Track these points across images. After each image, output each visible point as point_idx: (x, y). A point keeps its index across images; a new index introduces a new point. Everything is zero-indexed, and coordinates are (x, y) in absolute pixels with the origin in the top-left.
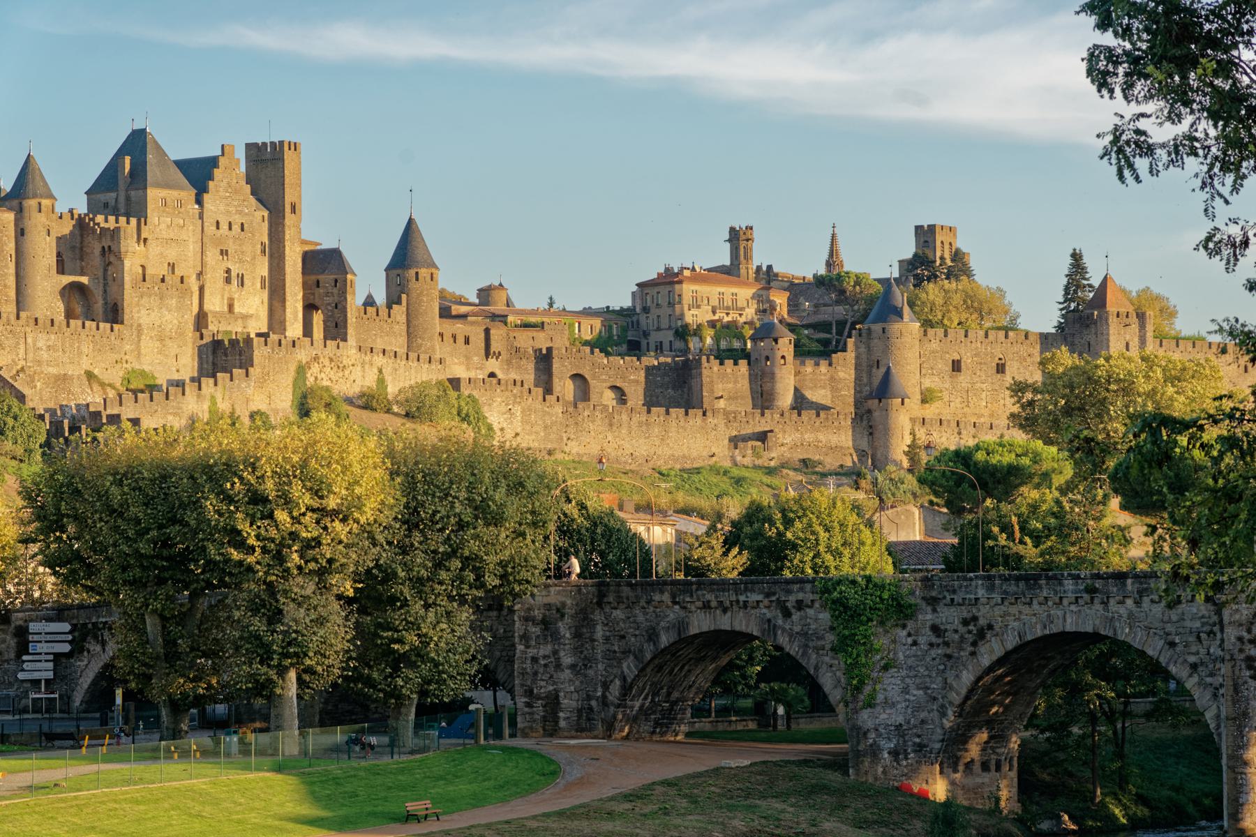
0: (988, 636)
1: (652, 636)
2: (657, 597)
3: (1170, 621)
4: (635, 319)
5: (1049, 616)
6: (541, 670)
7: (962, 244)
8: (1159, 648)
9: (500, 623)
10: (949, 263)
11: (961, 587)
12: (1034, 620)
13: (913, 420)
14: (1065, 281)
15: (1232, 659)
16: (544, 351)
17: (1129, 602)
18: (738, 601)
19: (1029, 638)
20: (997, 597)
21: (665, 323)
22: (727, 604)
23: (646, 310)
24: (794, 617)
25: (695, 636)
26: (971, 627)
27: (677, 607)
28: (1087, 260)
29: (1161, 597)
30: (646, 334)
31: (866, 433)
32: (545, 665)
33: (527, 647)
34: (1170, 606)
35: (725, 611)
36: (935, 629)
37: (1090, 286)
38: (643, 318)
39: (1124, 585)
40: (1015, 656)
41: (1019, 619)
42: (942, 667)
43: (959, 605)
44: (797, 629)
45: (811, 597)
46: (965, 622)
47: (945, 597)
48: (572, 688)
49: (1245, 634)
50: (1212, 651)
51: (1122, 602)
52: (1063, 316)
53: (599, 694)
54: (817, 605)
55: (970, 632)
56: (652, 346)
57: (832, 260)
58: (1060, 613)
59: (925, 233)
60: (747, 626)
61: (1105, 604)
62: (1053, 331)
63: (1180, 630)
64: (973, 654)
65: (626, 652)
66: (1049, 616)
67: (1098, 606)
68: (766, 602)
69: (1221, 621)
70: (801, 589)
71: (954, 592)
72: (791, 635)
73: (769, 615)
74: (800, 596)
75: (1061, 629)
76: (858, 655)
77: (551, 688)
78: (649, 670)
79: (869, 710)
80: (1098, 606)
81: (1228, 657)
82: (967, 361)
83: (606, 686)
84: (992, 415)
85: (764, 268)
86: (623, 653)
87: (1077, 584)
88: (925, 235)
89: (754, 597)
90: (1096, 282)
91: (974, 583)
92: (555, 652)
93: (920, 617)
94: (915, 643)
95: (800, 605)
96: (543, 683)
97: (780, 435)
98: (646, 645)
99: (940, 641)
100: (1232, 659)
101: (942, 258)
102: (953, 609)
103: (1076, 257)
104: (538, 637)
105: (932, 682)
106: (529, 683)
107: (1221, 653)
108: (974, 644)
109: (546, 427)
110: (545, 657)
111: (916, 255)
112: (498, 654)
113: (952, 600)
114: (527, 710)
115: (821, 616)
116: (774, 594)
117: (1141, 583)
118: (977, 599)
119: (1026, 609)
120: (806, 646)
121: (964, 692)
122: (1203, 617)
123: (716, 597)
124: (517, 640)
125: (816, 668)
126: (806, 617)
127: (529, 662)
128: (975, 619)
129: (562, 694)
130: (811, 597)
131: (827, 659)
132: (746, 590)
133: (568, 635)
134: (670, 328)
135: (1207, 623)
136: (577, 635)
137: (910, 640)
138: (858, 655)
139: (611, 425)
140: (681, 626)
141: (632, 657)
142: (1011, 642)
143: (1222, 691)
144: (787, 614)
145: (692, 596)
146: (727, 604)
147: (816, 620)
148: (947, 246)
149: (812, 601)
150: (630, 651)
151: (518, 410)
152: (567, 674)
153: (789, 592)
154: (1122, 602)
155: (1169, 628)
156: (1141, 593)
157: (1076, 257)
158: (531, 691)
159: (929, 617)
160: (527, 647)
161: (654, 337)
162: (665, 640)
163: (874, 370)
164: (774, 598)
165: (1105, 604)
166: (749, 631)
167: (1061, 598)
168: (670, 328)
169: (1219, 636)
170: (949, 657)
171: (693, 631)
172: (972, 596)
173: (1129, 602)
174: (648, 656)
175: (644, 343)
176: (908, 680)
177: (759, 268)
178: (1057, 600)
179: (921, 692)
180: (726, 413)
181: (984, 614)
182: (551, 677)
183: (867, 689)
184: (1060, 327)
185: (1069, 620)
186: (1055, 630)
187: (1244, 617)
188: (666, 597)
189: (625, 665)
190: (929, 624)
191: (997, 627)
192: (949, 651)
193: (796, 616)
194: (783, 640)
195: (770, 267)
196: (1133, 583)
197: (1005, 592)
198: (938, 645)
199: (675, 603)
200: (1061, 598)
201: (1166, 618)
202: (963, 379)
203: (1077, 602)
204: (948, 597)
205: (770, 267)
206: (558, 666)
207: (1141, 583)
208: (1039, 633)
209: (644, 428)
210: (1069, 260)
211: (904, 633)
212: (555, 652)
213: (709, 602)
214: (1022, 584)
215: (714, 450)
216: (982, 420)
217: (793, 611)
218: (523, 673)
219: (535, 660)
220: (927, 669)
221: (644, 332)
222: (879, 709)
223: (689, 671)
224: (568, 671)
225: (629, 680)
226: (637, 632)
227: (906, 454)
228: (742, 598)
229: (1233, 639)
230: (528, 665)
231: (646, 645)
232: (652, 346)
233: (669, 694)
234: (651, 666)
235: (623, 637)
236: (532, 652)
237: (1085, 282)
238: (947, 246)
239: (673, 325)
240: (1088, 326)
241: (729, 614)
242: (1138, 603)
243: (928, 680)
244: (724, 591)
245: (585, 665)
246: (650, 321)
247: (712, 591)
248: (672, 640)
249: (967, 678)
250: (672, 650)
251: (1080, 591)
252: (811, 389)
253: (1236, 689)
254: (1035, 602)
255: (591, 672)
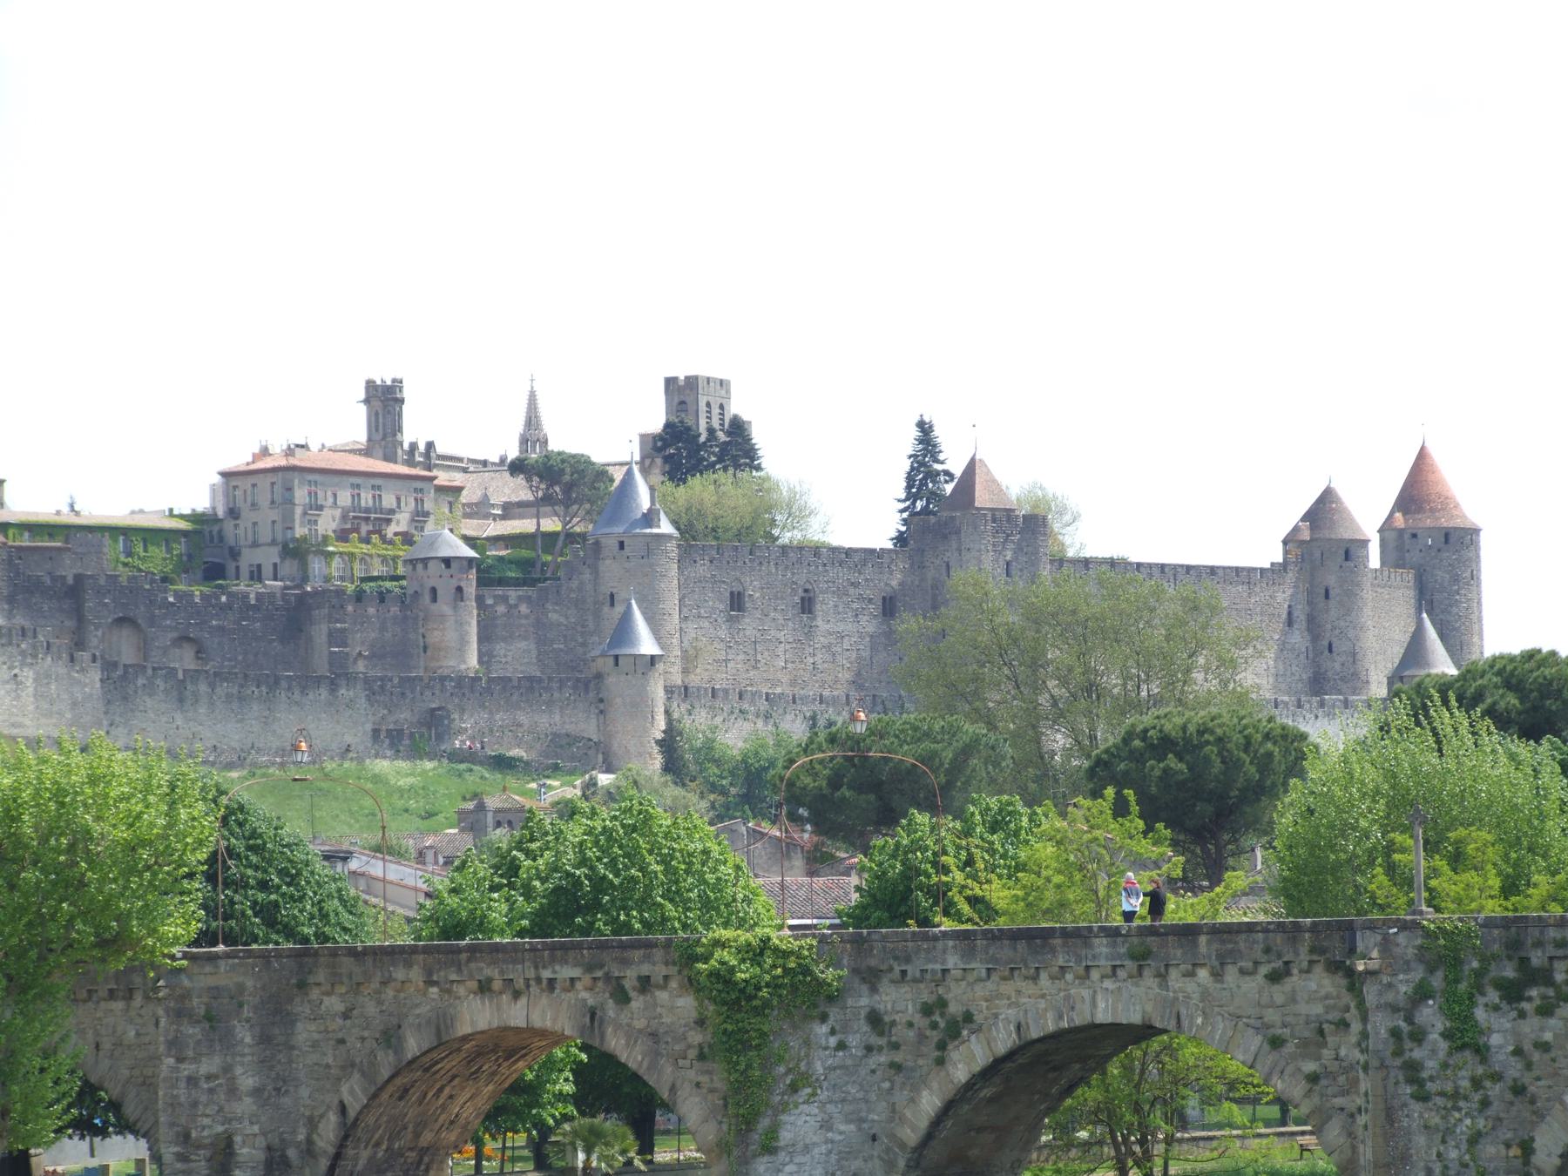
0: (965, 1033)
1: (390, 1037)
2: (400, 974)
3: (1272, 1005)
4: (216, 529)
5: (1067, 998)
6: (204, 1098)
7: (737, 407)
8: (1253, 1049)
9: (131, 1021)
10: (722, 437)
11: (918, 950)
12: (1042, 1004)
13: (669, 691)
14: (906, 465)
15: (1383, 1066)
16: (70, 581)
17: (1203, 973)
18: (538, 980)
19: (1035, 1034)
20: (979, 967)
21: (265, 535)
22: (520, 984)
23: (233, 513)
24: (634, 1004)
25: (465, 1039)
26: (937, 1018)
27: (434, 990)
28: (940, 434)
29: (1256, 963)
30: (235, 554)
31: (594, 711)
32: (211, 1091)
33: (180, 1060)
34: (1275, 977)
35: (517, 995)
36: (875, 1020)
37: (947, 473)
38: (229, 526)
39: (1195, 944)
40: (1009, 1065)
41: (1016, 1004)
42: (886, 1085)
43: (915, 981)
44: (639, 1024)
45: (664, 971)
46: (927, 1010)
47: (891, 969)
48: (256, 1128)
49: (1402, 1024)
50: (1343, 1052)
51: (1191, 974)
52: (905, 522)
53: (301, 1137)
54: (674, 984)
55: (934, 1026)
56: (245, 572)
57: (532, 431)
58: (1086, 993)
59: (680, 389)
60: (554, 1020)
61: (1162, 976)
62: (889, 545)
63: (1288, 1019)
64: (940, 1062)
65: (349, 1066)
66: (1067, 998)
67: (1149, 980)
68: (587, 979)
69: (1361, 1004)
70: (647, 958)
71: (908, 960)
72: (632, 1035)
73: (591, 1002)
74: (645, 969)
75: (1087, 1019)
76: (749, 1066)
77: (220, 1129)
78: (385, 1096)
79: (766, 1159)
80: (1149, 980)
81: (1374, 1063)
82: (753, 589)
83: (312, 1123)
84: (793, 683)
85: (422, 447)
86: (343, 1068)
87: (1114, 945)
88: (681, 392)
89: (566, 972)
90: (958, 470)
91: (940, 945)
92: (227, 1069)
93: (850, 1002)
94: (841, 1046)
95: (645, 984)
96: (206, 1121)
97: (456, 716)
98: (380, 1055)
99: (882, 1041)
100: (1383, 1066)
101: (711, 431)
102: (905, 989)
103: (925, 428)
104: (198, 1042)
105: (869, 1111)
106: (183, 1121)
107: (1362, 1058)
108: (942, 1046)
109: (74, 704)
110: (209, 1078)
111: (668, 426)
112: (126, 1072)
113: (904, 973)
114: (179, 1166)
115: (681, 1002)
116: (601, 966)
117: (1223, 942)
118: (945, 971)
119: (1028, 988)
120: (658, 1054)
121: (923, 1124)
122: (1327, 997)
123: (502, 972)
124: (162, 1048)
125: (673, 1089)
126: (655, 1005)
127: (183, 1084)
128: (942, 1003)
129: (238, 1139)
130: (664, 971)
131: (691, 1074)
132: (553, 960)
133: (248, 1040)
134: (274, 542)
135: (1334, 1007)
136: (264, 1039)
137: (833, 1041)
138: (749, 1066)
139: (181, 700)
140: (441, 1023)
141: (356, 1076)
142: (1004, 1041)
143: (1362, 1120)
144: (622, 998)
145: (459, 971)
146: (520, 984)
147: (672, 1008)
148: (716, 411)
149: (666, 978)
150: (353, 1065)
151: (28, 676)
152: (246, 1105)
153: (625, 962)
154: (1191, 974)
155: (1271, 1016)
156: (1223, 960)
157: (925, 428)
158: (187, 1136)
159: (864, 1001)
160: (180, 1060)
161: (248, 558)
162: (413, 1045)
163: (606, 609)
164: (599, 974)
165: (1162, 976)
166: (558, 1028)
167: (1088, 968)
168: (274, 542)
169: (1356, 1027)
170: (896, 1067)
171: (464, 1029)
172: (938, 967)
173: (1203, 973)
174: (385, 1073)
175: (231, 567)
176: (830, 1108)
177: (414, 446)
178: (1081, 971)
179: (852, 1127)
180: (368, 682)
181: (958, 997)
182: (221, 1110)
183: (764, 1123)
184: (900, 539)
185: (1101, 1005)
186: (1078, 1022)
187: (1401, 997)
188: (416, 974)
189: (345, 1089)
190: (863, 1013)
191: (978, 1018)
192: (898, 1057)
193: (637, 1003)
194: (615, 1043)
195: (430, 445)
196: (1209, 943)
197: (995, 960)
198: (880, 1049)
199: (430, 983)
200: (1088, 968)
201: (1265, 1000)
202: (749, 625)
203: (1114, 974)
204: (897, 969)
205: (430, 445)
206: (232, 1091)
207: (1223, 942)
208: (1051, 1027)
209: (235, 705)
210: (915, 433)
211: (824, 1029)
212: (227, 1069)
213: (490, 980)
214: (1022, 946)
215: (349, 739)
216: (779, 690)
217: (632, 994)
218: (173, 1104)
219: (192, 1081)
220: (862, 1087)
221: (231, 549)
222: (782, 1156)
223: (451, 1097)
224: (248, 1100)
225: (352, 1114)
226: (366, 1034)
227: (658, 742)
228: (546, 974)
229: (1383, 1033)
230: (182, 1092)
231: (380, 1055)
232: (245, 572)
233: (417, 1135)
234: (390, 1089)
235: (342, 1041)
236: (187, 1069)
237: (938, 467)
238: (716, 411)
239: (279, 538)
240: (945, 537)
241: (523, 1001)
242: (1217, 975)
243: (863, 1106)
244: (515, 962)
245: (278, 1090)
246: (241, 532)
247: (494, 963)
248: (426, 1046)
249: (929, 1102)
250: (423, 1065)
251: (1120, 957)
252: (504, 639)
253: (1390, 1115)
254: (1044, 975)
255: (286, 1101)
